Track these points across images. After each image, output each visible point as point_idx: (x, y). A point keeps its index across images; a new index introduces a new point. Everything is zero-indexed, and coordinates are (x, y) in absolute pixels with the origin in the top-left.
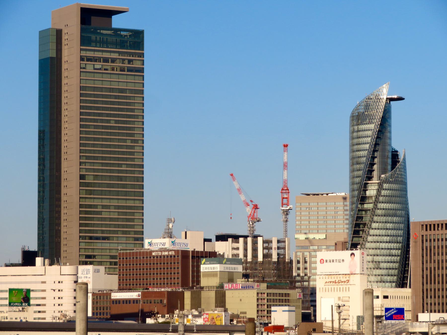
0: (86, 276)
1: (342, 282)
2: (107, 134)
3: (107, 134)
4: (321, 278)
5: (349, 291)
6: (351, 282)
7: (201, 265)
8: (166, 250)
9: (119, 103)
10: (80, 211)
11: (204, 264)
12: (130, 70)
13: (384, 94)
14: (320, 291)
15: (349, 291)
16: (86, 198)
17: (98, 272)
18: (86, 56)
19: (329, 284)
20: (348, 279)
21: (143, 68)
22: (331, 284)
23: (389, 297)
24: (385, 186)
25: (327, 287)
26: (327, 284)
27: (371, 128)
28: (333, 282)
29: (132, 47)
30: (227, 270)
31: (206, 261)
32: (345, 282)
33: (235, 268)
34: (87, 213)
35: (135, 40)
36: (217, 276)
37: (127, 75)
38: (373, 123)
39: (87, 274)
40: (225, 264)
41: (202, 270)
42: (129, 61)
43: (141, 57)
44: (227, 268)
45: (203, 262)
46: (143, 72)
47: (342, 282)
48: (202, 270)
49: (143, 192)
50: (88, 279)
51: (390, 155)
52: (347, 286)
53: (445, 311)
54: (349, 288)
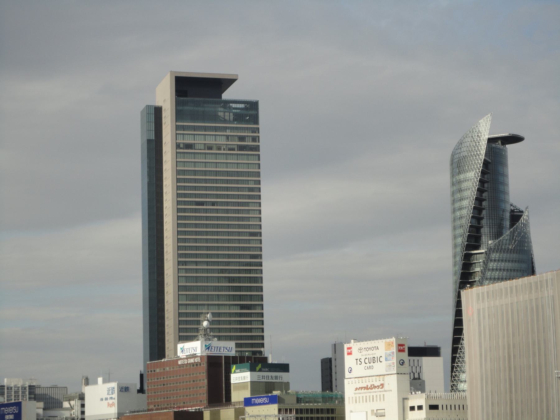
0: (111, 396)
1: (375, 387)
2: (213, 226)
3: (213, 226)
4: (350, 382)
5: (384, 400)
6: (386, 387)
7: (232, 375)
8: (194, 356)
9: (227, 189)
10: (179, 321)
11: (235, 372)
12: (241, 148)
13: (485, 130)
14: (349, 403)
15: (384, 400)
16: (186, 305)
17: (125, 391)
18: (216, 144)
19: (360, 391)
20: (382, 382)
21: (259, 146)
22: (363, 390)
23: (440, 407)
24: (494, 256)
25: (357, 396)
26: (358, 391)
27: (472, 177)
28: (365, 388)
29: (248, 122)
30: (263, 380)
31: (236, 368)
32: (378, 386)
33: (276, 377)
34: (187, 322)
35: (250, 112)
36: (248, 389)
37: (237, 154)
38: (473, 170)
39: (112, 394)
40: (260, 370)
41: (232, 381)
42: (239, 138)
43: (255, 133)
44: (263, 377)
45: (233, 370)
46: (259, 151)
47: (375, 387)
48: (232, 382)
49: (262, 295)
50: (113, 401)
51: (508, 215)
52: (382, 394)
53: (299, 415)
54: (384, 395)
